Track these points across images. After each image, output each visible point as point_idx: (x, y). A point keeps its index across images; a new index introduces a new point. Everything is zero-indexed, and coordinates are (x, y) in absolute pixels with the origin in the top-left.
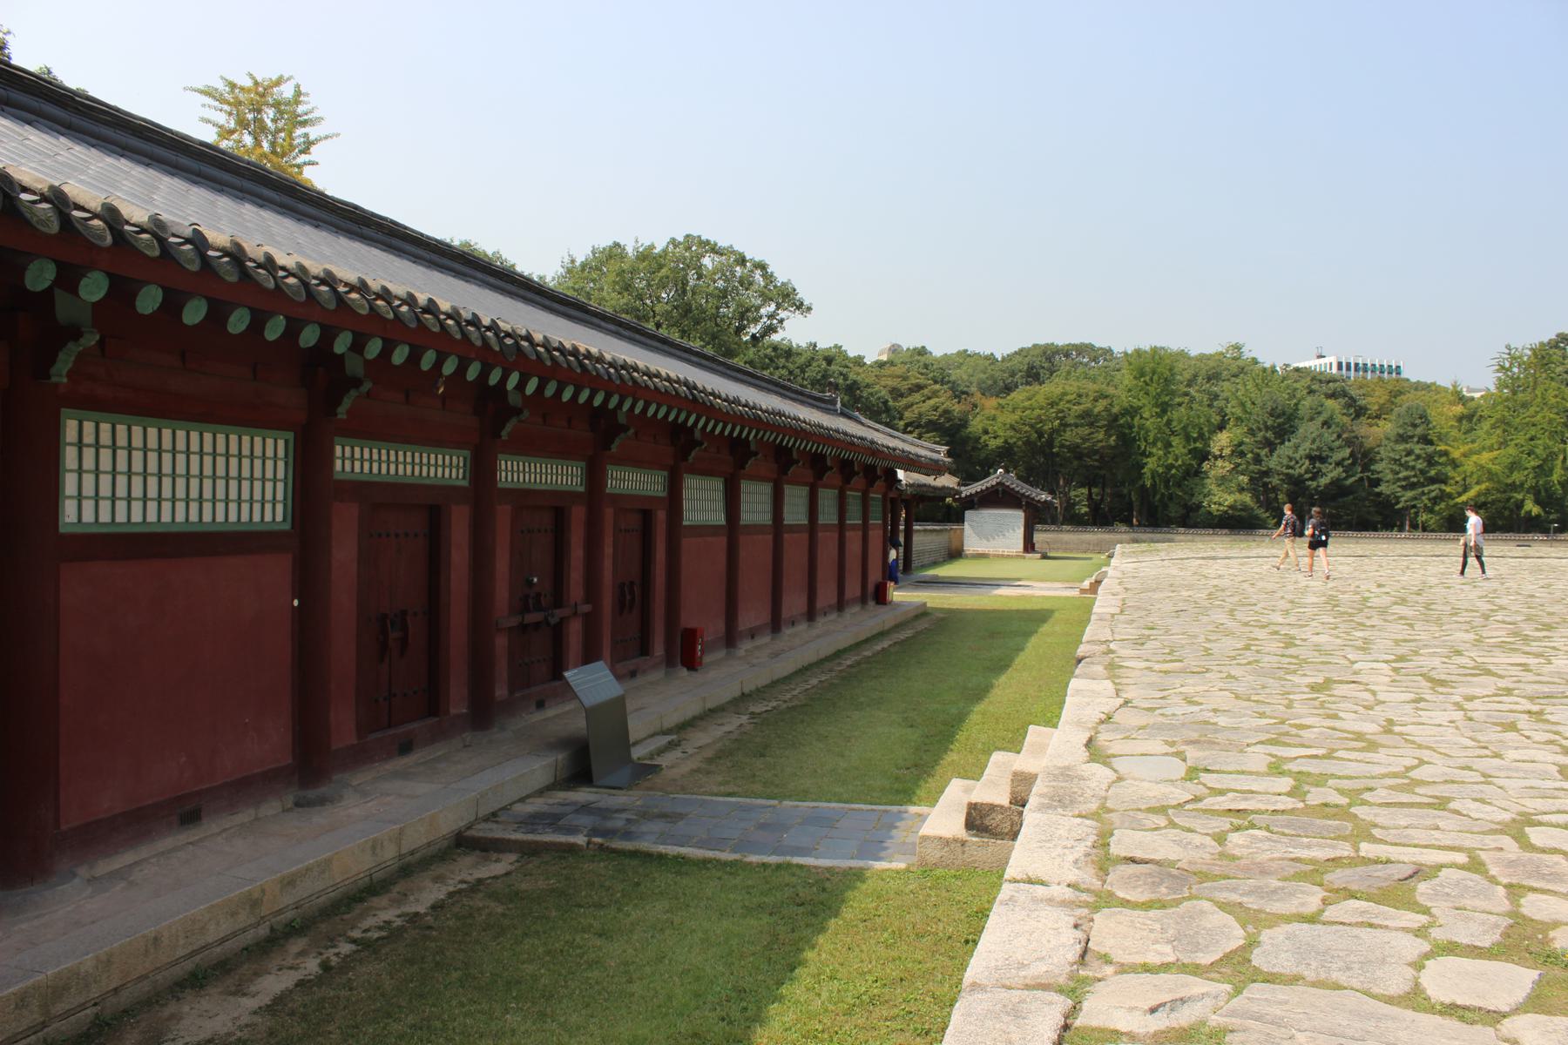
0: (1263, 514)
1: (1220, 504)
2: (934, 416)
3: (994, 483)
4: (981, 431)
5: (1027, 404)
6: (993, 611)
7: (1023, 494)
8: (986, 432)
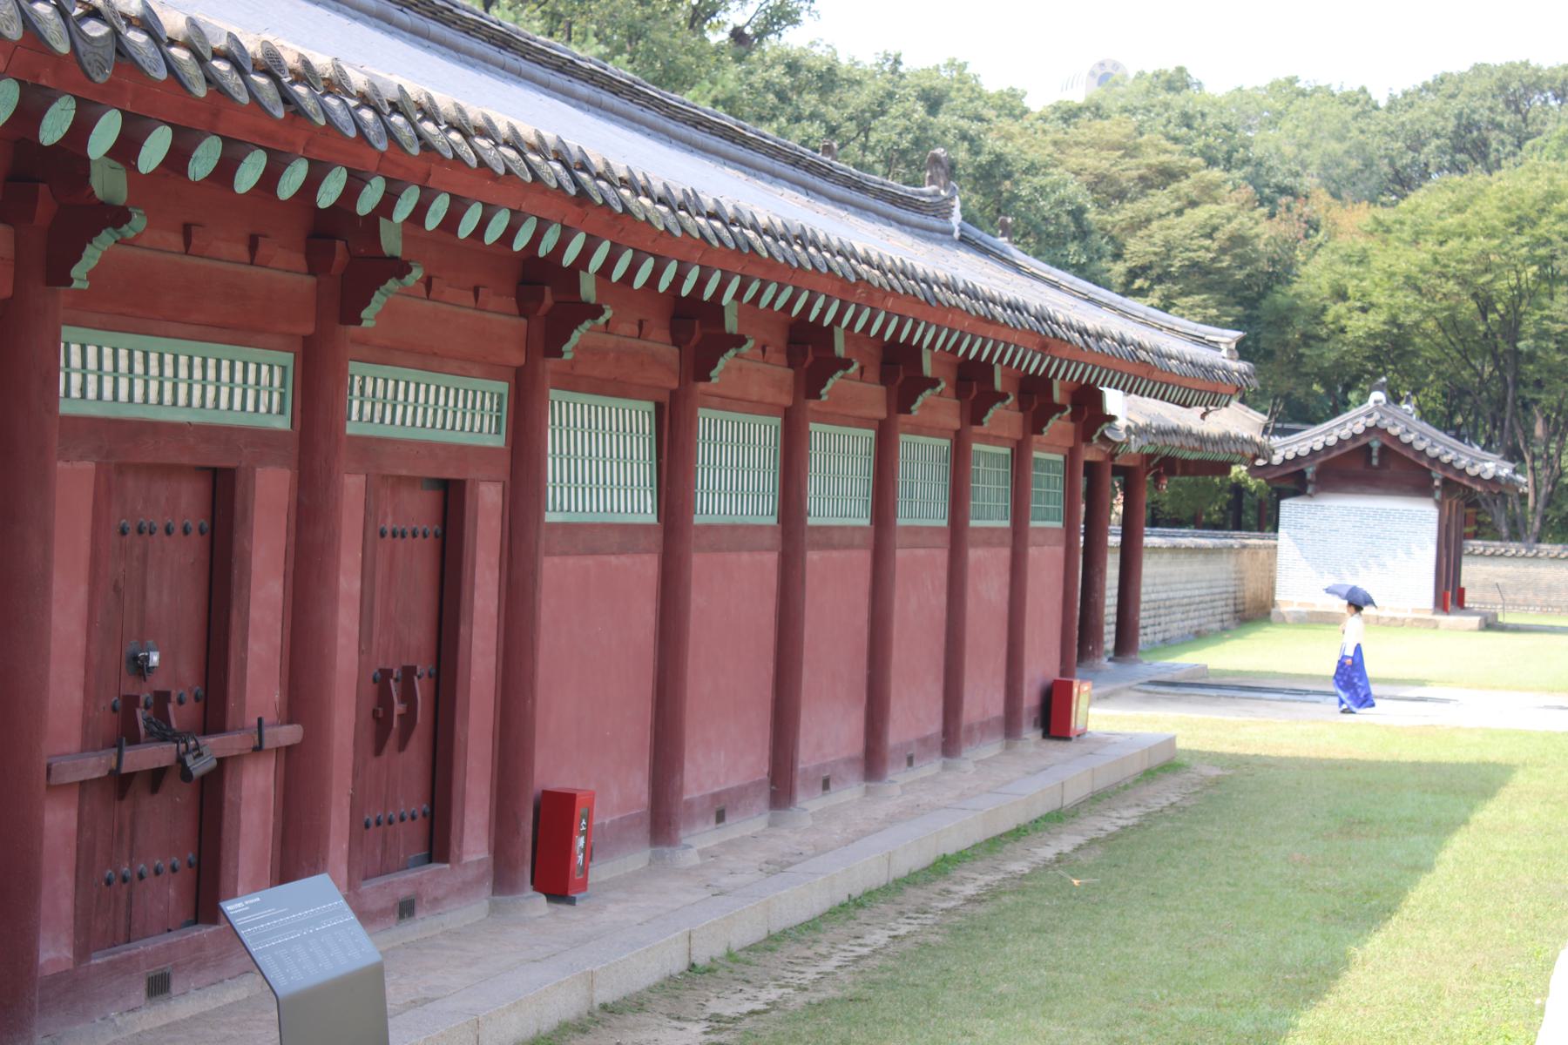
3: (1359, 429)
5: (1452, 221)
8: (1341, 295)
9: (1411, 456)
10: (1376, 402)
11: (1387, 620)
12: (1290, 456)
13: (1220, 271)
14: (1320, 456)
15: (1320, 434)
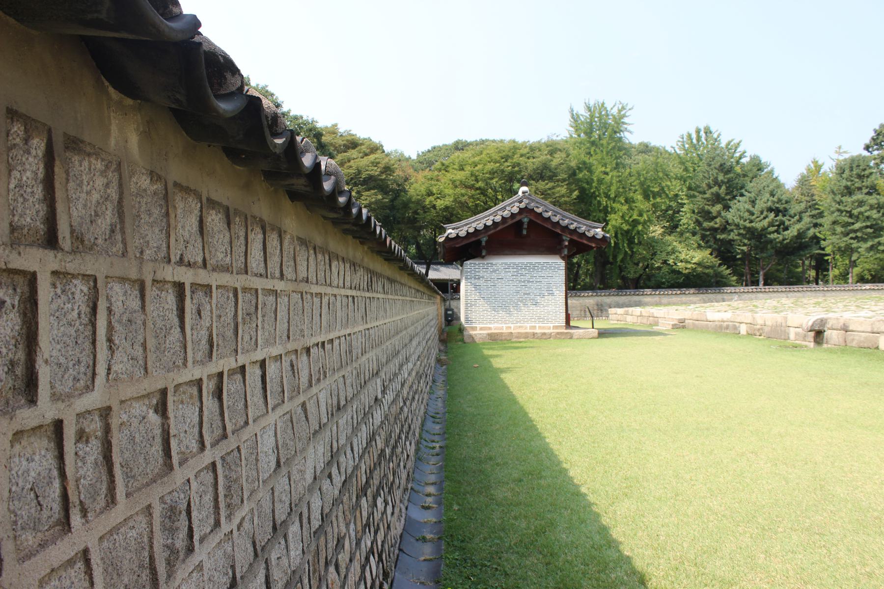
0: (725, 271)
1: (687, 262)
2: (375, 171)
3: (515, 210)
4: (425, 193)
5: (477, 159)
6: (577, 494)
7: (566, 228)
8: (430, 194)
9: (549, 227)
10: (523, 193)
11: (539, 335)
12: (471, 230)
13: (381, 180)
14: (490, 230)
15: (489, 216)
